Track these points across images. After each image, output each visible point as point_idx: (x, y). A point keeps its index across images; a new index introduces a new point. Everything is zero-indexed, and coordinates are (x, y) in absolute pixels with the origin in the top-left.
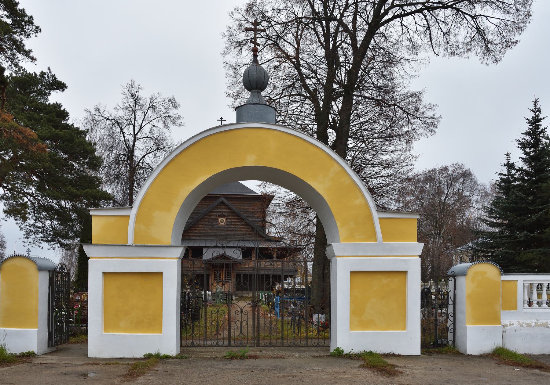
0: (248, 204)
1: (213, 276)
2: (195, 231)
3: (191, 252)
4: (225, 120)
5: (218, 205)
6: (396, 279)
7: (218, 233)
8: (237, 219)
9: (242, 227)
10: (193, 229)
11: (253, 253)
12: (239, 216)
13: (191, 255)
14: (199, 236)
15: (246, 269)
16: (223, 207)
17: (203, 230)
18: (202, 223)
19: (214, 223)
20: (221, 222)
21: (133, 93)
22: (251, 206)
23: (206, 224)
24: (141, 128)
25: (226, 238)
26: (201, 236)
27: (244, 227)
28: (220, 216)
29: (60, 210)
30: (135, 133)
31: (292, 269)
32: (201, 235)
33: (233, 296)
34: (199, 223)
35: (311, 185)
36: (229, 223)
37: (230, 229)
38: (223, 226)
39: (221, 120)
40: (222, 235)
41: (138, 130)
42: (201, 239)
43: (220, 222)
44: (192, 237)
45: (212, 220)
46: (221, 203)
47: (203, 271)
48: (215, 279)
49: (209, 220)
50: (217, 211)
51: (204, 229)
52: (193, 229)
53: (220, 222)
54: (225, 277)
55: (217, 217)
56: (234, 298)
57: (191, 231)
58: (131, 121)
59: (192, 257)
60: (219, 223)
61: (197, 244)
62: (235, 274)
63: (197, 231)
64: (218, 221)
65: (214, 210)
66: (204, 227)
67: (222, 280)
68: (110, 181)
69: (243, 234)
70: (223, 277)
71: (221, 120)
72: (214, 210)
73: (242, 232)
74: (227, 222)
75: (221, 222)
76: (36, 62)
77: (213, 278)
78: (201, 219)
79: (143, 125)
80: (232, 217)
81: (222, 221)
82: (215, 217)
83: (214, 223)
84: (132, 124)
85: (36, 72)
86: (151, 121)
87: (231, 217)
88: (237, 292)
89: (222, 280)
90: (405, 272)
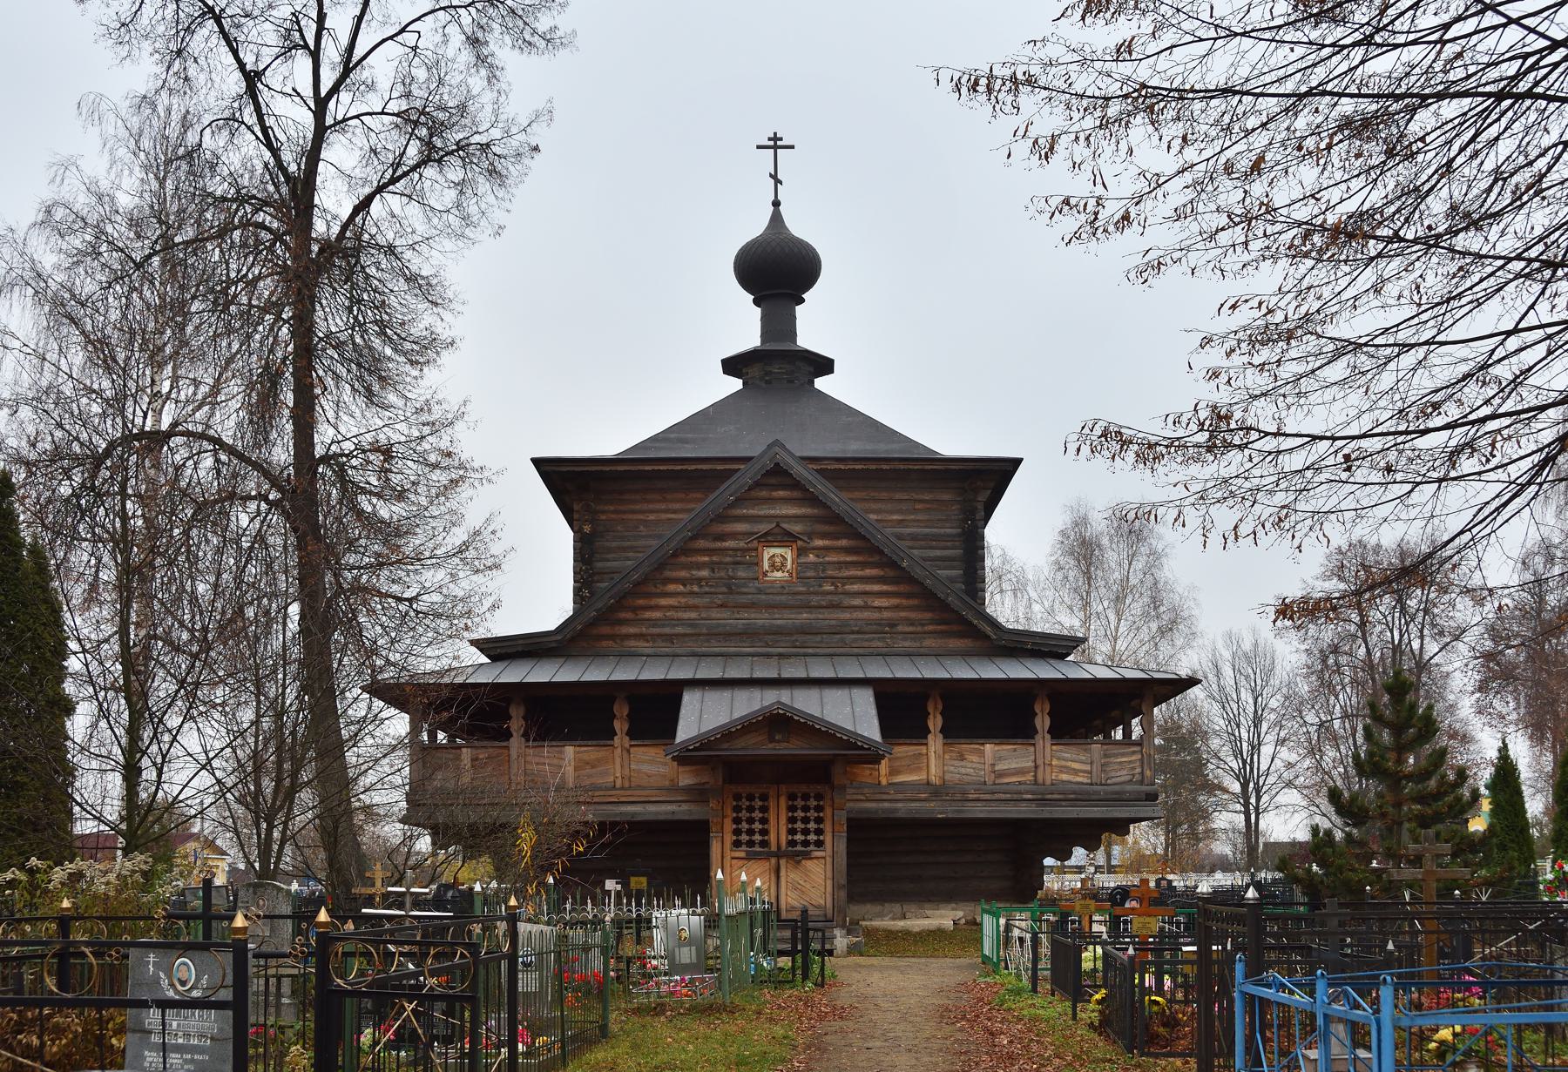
0: (901, 501)
1: (729, 826)
2: (648, 615)
3: (626, 712)
4: (792, 147)
5: (757, 485)
7: (761, 619)
8: (847, 550)
9: (876, 588)
10: (641, 602)
11: (930, 710)
12: (858, 536)
13: (626, 727)
14: (670, 638)
15: (897, 792)
16: (781, 493)
17: (688, 607)
18: (683, 574)
19: (741, 574)
20: (773, 567)
22: (915, 511)
23: (699, 580)
24: (348, 67)
25: (801, 640)
26: (677, 635)
27: (885, 588)
28: (768, 539)
30: (323, 92)
31: (1129, 788)
32: (680, 630)
33: (837, 932)
34: (668, 574)
36: (811, 573)
37: (815, 600)
38: (783, 588)
39: (775, 147)
40: (778, 632)
41: (335, 76)
42: (679, 651)
43: (766, 566)
44: (632, 643)
45: (728, 559)
46: (769, 473)
47: (685, 807)
48: (737, 844)
49: (715, 558)
50: (751, 512)
51: (692, 601)
52: (641, 602)
53: (766, 566)
54: (792, 832)
55: (755, 543)
56: (841, 941)
57: (629, 615)
58: (300, 30)
59: (632, 734)
60: (765, 574)
61: (654, 672)
62: (842, 816)
63: (657, 614)
64: (757, 563)
65: (738, 512)
66: (692, 593)
67: (774, 848)
69: (879, 623)
70: (778, 833)
71: (775, 147)
72: (738, 512)
73: (876, 615)
74: (801, 567)
75: (773, 567)
77: (729, 838)
78: (675, 555)
79: (359, 52)
80: (827, 543)
81: (778, 563)
82: (742, 544)
83: (741, 574)
84: (306, 46)
86: (403, 31)
87: (819, 543)
88: (856, 910)
89: (774, 848)
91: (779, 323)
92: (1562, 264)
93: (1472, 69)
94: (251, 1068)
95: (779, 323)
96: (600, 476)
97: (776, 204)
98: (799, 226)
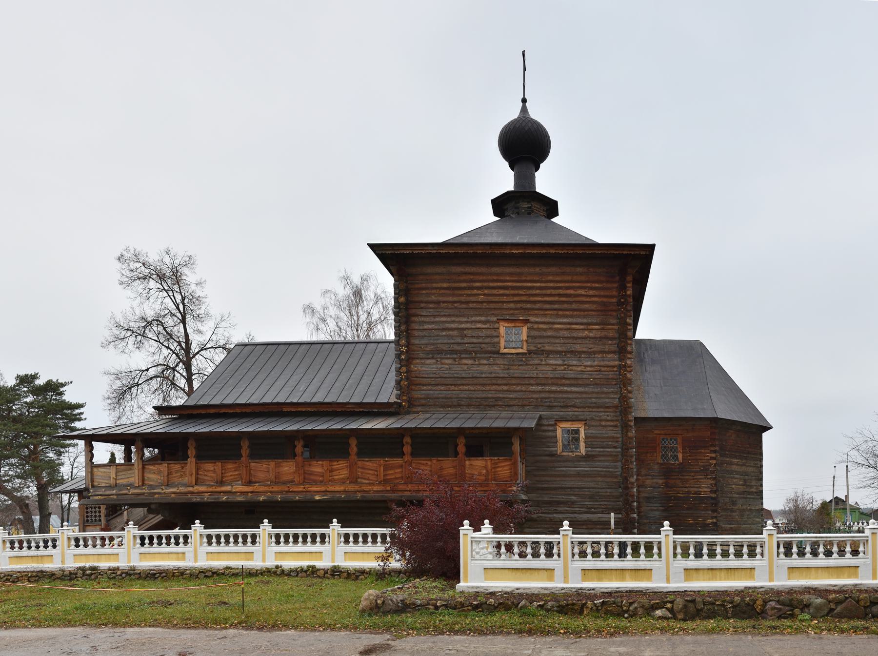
6: (50, 558)
21: (126, 328)
29: (48, 397)
35: (536, 179)
68: (677, 459)
76: (342, 274)
85: (84, 408)
90: (651, 569)
91: (525, 179)
92: (4, 446)
93: (439, 360)
94: (2, 528)
95: (525, 179)
96: (420, 256)
97: (524, 101)
98: (535, 114)
